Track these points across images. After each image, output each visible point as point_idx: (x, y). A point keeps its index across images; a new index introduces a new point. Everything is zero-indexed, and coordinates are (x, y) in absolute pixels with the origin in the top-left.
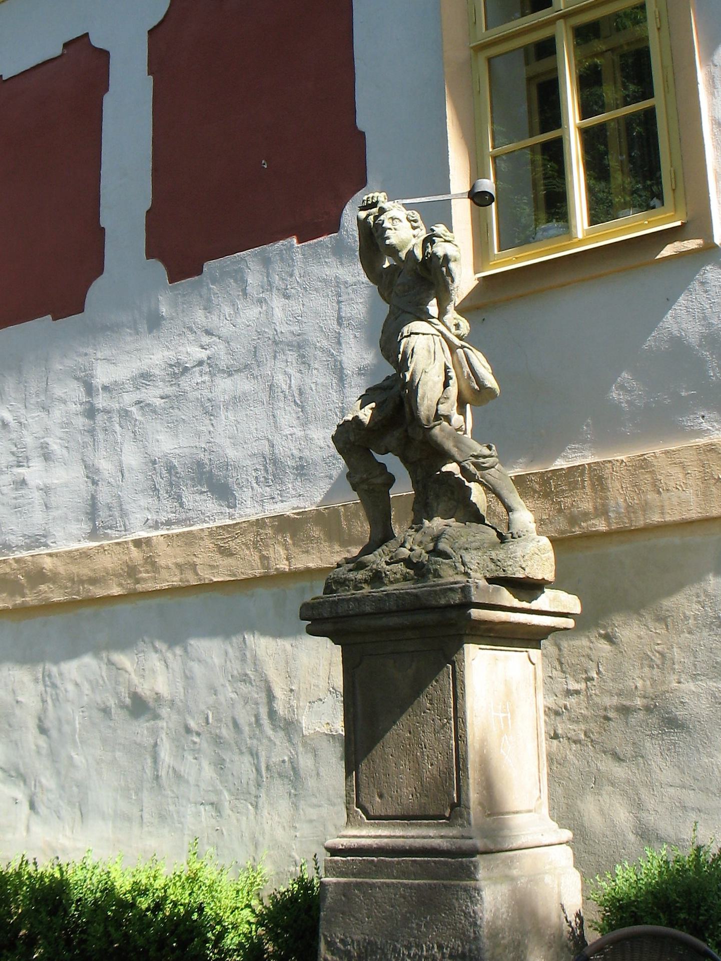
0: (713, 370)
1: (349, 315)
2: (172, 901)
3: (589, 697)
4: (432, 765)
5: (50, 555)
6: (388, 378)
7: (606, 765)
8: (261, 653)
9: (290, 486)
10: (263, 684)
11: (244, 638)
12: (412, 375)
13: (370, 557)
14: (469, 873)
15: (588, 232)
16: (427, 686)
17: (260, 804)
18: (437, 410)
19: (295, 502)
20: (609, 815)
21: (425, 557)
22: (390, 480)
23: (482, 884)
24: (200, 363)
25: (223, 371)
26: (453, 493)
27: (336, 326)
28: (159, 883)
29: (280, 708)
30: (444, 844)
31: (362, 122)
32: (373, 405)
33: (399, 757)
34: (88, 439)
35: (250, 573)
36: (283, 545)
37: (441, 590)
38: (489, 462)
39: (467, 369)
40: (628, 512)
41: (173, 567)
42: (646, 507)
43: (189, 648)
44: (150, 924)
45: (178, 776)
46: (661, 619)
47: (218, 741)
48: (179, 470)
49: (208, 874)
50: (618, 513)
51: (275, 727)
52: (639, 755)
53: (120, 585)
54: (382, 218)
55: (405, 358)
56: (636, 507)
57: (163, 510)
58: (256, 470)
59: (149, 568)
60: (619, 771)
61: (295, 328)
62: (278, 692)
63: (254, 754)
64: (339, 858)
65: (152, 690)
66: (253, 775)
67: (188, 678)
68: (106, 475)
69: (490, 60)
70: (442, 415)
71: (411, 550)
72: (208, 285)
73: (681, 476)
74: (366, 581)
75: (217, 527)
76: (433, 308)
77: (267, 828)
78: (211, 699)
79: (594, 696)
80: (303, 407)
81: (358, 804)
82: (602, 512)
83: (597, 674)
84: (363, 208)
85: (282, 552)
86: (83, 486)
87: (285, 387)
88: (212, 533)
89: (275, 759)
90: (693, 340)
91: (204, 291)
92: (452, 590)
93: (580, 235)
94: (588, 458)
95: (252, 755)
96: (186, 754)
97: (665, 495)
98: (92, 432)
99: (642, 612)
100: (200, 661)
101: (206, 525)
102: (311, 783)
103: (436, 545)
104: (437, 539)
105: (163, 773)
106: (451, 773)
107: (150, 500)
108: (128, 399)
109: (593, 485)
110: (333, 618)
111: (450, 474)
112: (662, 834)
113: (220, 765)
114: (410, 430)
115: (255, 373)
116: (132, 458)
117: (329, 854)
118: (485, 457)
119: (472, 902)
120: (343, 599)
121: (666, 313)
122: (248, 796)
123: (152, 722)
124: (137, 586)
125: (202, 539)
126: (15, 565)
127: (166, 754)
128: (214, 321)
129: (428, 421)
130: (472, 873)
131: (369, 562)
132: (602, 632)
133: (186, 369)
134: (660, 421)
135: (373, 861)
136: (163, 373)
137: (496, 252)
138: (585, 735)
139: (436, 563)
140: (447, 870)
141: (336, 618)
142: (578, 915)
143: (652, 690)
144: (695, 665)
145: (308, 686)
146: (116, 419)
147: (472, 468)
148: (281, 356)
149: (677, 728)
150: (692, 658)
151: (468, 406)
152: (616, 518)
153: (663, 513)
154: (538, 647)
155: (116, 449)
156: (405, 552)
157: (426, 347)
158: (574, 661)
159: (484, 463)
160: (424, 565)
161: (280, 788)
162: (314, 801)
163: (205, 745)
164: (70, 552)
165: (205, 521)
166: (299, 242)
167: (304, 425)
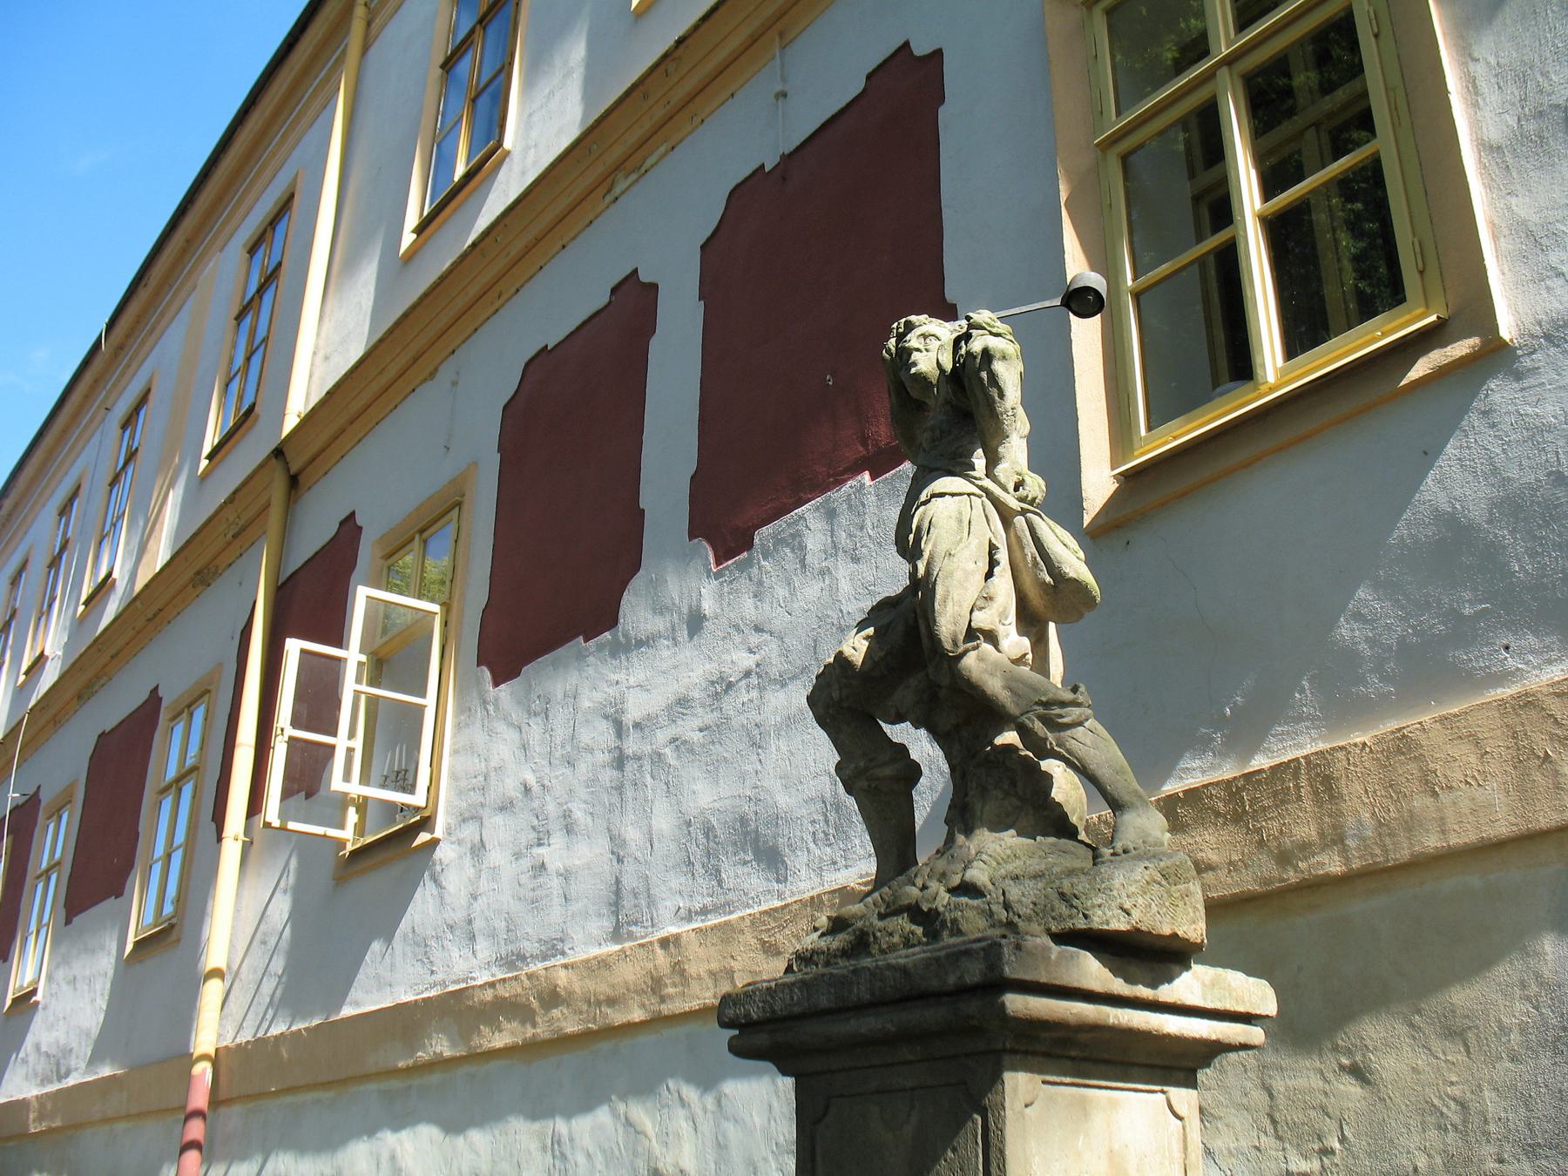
0: (1519, 560)
5: (565, 966)
15: (1283, 372)
16: (936, 1160)
24: (748, 674)
26: (1013, 784)
34: (615, 799)
37: (948, 956)
39: (1031, 549)
42: (1411, 823)
43: (723, 1101)
46: (1454, 1032)
50: (1363, 839)
53: (643, 1006)
56: (1394, 824)
59: (677, 979)
65: (676, 1165)
67: (721, 1146)
68: (633, 848)
69: (1125, 159)
70: (981, 631)
73: (1473, 759)
76: (979, 460)
82: (1335, 839)
86: (607, 867)
88: (755, 921)
90: (1477, 512)
91: (755, 570)
93: (1271, 378)
97: (1445, 798)
98: (620, 788)
101: (749, 911)
107: (683, 879)
108: (662, 736)
109: (1316, 793)
110: (769, 1021)
111: (1010, 748)
116: (664, 822)
118: (1063, 704)
125: (742, 931)
126: (527, 983)
129: (955, 643)
132: (1345, 1061)
133: (730, 685)
134: (1427, 667)
137: (1143, 432)
146: (647, 767)
147: (1038, 727)
150: (1522, 1110)
151: (1052, 626)
154: (1191, 1083)
155: (646, 813)
157: (954, 514)
158: (1298, 1117)
159: (1061, 716)
160: (938, 913)
164: (587, 961)
165: (748, 906)
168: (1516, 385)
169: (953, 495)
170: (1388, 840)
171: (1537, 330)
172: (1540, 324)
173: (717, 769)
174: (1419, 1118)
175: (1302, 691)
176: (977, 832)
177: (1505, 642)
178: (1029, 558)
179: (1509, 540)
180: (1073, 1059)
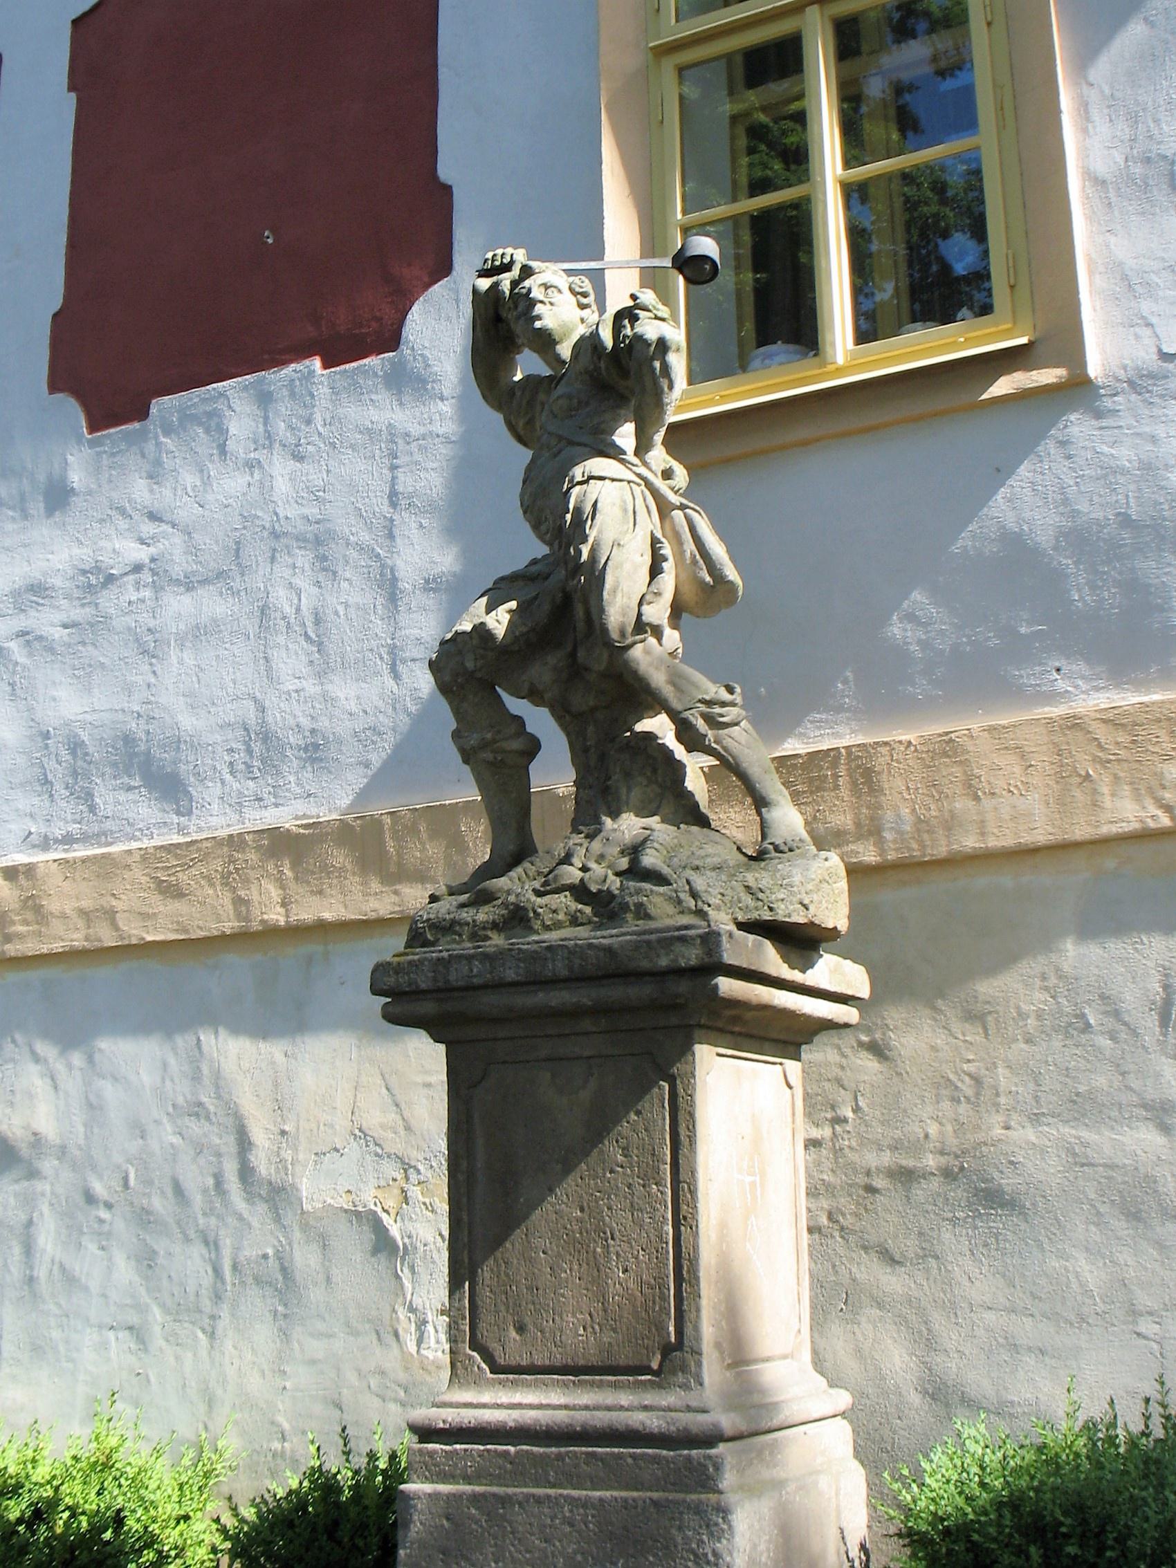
0: (1079, 590)
1: (411, 489)
2: (68, 1508)
3: (837, 1152)
4: (625, 1271)
6: (534, 562)
7: (869, 1271)
8: (229, 1066)
9: (292, 778)
10: (230, 1121)
11: (199, 1040)
12: (593, 551)
13: (502, 882)
14: (704, 1479)
16: (617, 1121)
17: (219, 1332)
18: (640, 615)
19: (300, 807)
20: (873, 1358)
21: (614, 883)
22: (533, 747)
23: (731, 1498)
24: (137, 568)
25: (178, 582)
26: (655, 771)
27: (386, 509)
28: (41, 1473)
29: (262, 1163)
30: (653, 1422)
31: (446, 171)
32: (513, 605)
33: (559, 1255)
35: (214, 928)
36: (277, 880)
37: (659, 941)
38: (731, 714)
39: (690, 546)
40: (918, 830)
41: (73, 915)
42: (950, 823)
43: (97, 1057)
44: (24, 1549)
45: (70, 1280)
46: (975, 1016)
47: (144, 1218)
48: (91, 750)
49: (132, 1457)
50: (901, 833)
51: (250, 1197)
52: (929, 1253)
54: (527, 283)
55: (579, 521)
56: (934, 822)
57: (59, 818)
58: (231, 750)
59: (30, 916)
60: (892, 1282)
61: (313, 511)
62: (260, 1136)
63: (210, 1243)
64: (437, 1446)
65: (26, 1127)
66: (208, 1279)
67: (94, 1108)
71: (584, 869)
72: (156, 437)
73: (1017, 770)
74: (495, 926)
75: (156, 848)
76: (625, 436)
77: (231, 1372)
78: (134, 1146)
79: (847, 1150)
80: (320, 644)
81: (478, 1344)
83: (854, 1111)
84: (484, 273)
85: (275, 893)
87: (289, 610)
89: (249, 1252)
90: (1044, 538)
91: (150, 447)
92: (683, 940)
93: (840, 360)
94: (841, 736)
95: (206, 1243)
96: (85, 1240)
97: (987, 803)
99: (940, 1003)
100: (116, 1079)
101: (135, 845)
102: (316, 1295)
103: (635, 862)
104: (635, 850)
105: (41, 1273)
106: (663, 1286)
107: (36, 801)
109: (854, 783)
110: (439, 990)
111: (650, 737)
112: (972, 1392)
113: (147, 1260)
114: (581, 654)
115: (237, 584)
117: (415, 1438)
118: (723, 704)
119: (711, 1535)
120: (460, 957)
121: (995, 493)
122: (198, 1316)
123: (26, 1184)
124: (7, 947)
127: (47, 1239)
128: (165, 496)
129: (623, 634)
130: (709, 1478)
131: (500, 890)
132: (864, 1038)
133: (110, 579)
134: (979, 675)
135: (507, 1452)
136: (68, 584)
138: (830, 1217)
139: (639, 892)
140: (659, 1473)
141: (443, 991)
142: (863, 1547)
143: (955, 1142)
144: (1037, 1099)
145: (314, 1126)
147: (701, 724)
148: (283, 558)
149: (1002, 1206)
150: (1031, 1086)
152: (895, 841)
153: (983, 834)
156: (572, 874)
157: (618, 502)
160: (613, 896)
161: (256, 1303)
162: (320, 1326)
163: (120, 1225)
165: (134, 838)
166: (326, 366)
167: (321, 675)
168: (1094, 422)
169: (613, 480)
170: (926, 836)
171: (1122, 374)
172: (1125, 368)
173: (89, 675)
174: (934, 1091)
175: (845, 682)
176: (624, 816)
177: (1057, 664)
178: (688, 555)
179: (1072, 569)
180: (732, 1033)
